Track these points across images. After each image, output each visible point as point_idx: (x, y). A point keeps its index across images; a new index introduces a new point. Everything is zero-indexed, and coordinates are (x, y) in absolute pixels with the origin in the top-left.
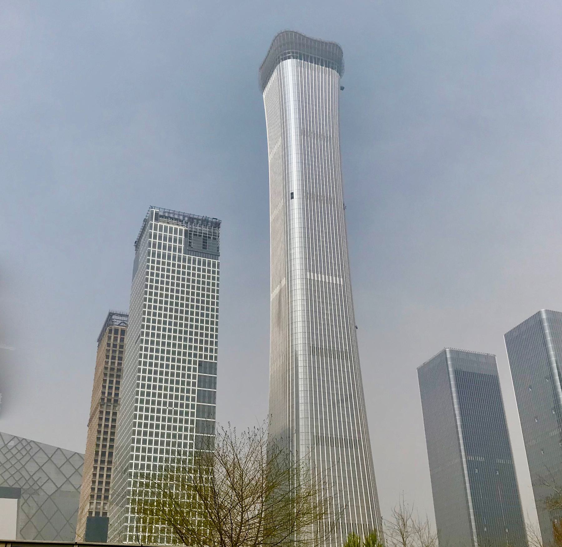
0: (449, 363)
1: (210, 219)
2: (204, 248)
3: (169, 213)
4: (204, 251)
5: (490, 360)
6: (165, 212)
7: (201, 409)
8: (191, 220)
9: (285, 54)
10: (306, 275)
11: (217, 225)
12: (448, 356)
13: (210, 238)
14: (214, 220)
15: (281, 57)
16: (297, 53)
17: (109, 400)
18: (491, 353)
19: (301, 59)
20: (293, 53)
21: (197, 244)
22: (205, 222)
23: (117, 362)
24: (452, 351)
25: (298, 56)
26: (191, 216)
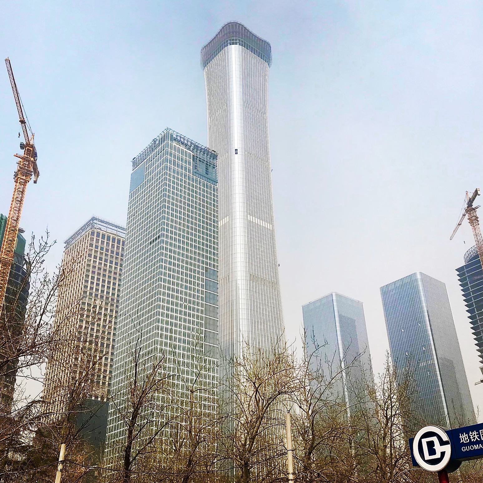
0: (335, 304)
1: (210, 151)
2: (206, 173)
3: (181, 137)
4: (206, 176)
5: (358, 307)
6: (177, 136)
7: (208, 296)
8: (196, 147)
9: (233, 40)
10: (247, 217)
11: (215, 157)
12: (334, 298)
13: (210, 166)
14: (213, 152)
15: (229, 42)
16: (242, 41)
17: (91, 294)
18: (361, 301)
19: (245, 47)
20: (239, 40)
21: (202, 169)
22: (205, 151)
23: (98, 261)
24: (337, 295)
25: (244, 45)
26: (197, 144)
